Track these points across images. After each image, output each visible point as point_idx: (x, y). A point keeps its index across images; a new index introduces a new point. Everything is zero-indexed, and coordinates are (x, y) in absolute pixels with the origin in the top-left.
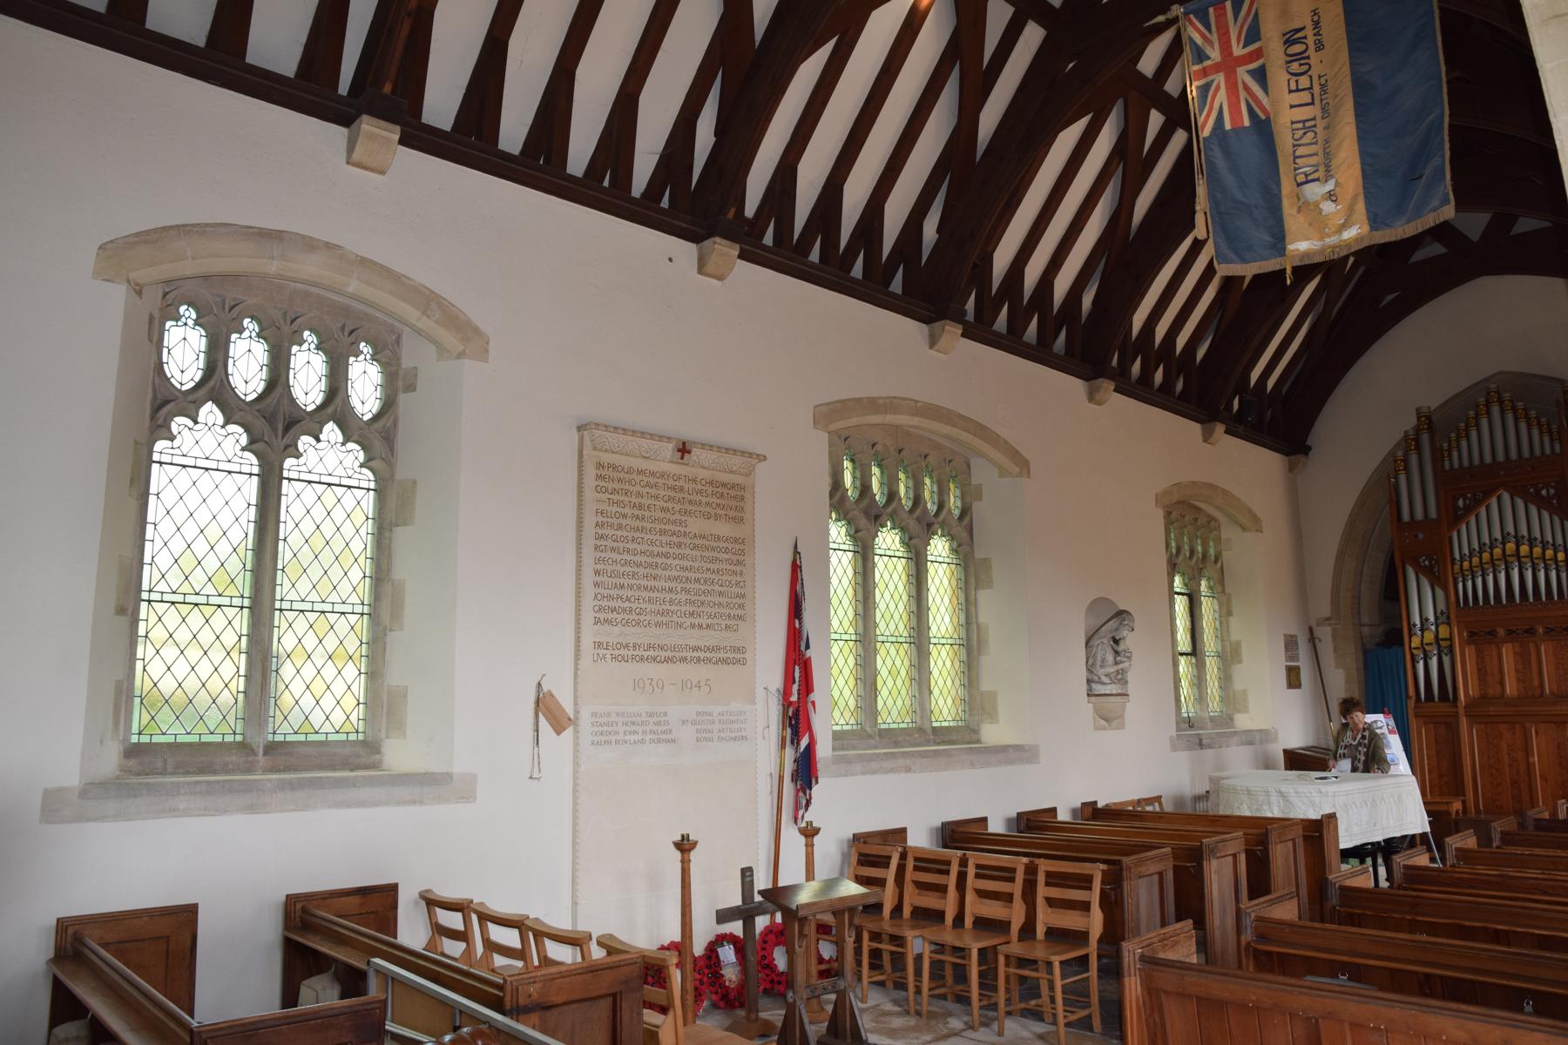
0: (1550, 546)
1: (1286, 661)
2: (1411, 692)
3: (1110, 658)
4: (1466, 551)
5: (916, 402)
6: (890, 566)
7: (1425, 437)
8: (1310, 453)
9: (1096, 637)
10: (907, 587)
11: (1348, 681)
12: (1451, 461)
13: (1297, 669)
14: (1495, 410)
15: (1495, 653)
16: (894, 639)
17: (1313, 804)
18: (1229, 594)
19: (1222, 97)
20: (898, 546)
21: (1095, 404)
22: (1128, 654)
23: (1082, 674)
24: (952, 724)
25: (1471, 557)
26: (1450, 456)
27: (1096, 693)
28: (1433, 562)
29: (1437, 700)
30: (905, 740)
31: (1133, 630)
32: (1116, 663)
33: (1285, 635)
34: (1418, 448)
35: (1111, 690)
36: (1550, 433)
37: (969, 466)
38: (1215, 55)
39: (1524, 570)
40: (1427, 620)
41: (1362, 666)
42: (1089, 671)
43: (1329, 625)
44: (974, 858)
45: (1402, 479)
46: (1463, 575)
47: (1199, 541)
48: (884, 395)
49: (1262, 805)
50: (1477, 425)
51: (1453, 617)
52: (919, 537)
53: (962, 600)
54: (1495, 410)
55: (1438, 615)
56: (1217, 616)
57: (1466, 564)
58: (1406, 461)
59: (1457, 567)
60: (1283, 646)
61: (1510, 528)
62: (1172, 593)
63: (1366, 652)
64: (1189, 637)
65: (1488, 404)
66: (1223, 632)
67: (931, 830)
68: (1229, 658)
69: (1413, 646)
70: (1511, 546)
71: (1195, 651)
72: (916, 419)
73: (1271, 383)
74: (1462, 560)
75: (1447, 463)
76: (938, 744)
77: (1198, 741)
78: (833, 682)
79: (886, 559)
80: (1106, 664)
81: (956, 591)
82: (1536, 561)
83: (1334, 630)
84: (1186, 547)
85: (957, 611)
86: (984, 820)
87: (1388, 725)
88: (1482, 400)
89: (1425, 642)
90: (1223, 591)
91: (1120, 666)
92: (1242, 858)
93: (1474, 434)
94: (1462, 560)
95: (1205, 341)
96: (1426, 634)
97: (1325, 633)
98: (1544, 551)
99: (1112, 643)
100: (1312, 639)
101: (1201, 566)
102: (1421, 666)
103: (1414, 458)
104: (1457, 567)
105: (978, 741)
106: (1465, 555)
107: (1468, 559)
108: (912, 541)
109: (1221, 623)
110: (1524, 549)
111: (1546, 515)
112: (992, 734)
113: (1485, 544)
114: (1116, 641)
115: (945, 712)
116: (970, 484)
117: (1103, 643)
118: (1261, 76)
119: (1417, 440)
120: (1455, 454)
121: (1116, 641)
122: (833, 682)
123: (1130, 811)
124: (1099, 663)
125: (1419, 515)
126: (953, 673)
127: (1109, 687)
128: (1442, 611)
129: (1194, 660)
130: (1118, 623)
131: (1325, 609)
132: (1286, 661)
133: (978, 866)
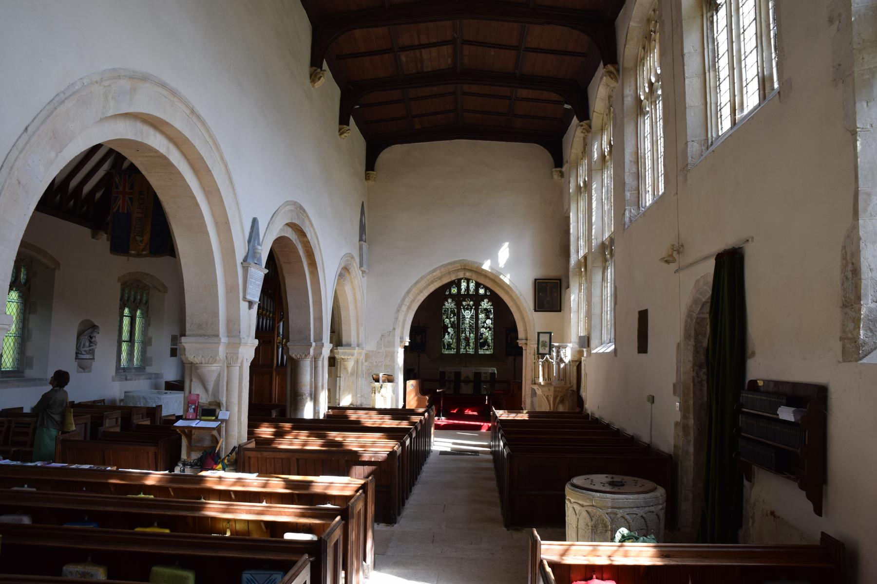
1: (171, 345)
3: (87, 344)
17: (155, 402)
19: (120, 202)
24: (11, 369)
32: (90, 346)
38: (121, 189)
47: (139, 294)
53: (22, 318)
56: (143, 325)
62: (122, 316)
64: (129, 334)
66: (144, 332)
68: (146, 343)
71: (131, 340)
76: (3, 378)
84: (132, 297)
86: (22, 408)
90: (147, 316)
91: (91, 348)
92: (120, 419)
98: (270, 314)
105: (23, 377)
109: (145, 329)
114: (91, 337)
118: (131, 199)
124: (82, 346)
126: (14, 348)
127: (85, 356)
129: (130, 344)
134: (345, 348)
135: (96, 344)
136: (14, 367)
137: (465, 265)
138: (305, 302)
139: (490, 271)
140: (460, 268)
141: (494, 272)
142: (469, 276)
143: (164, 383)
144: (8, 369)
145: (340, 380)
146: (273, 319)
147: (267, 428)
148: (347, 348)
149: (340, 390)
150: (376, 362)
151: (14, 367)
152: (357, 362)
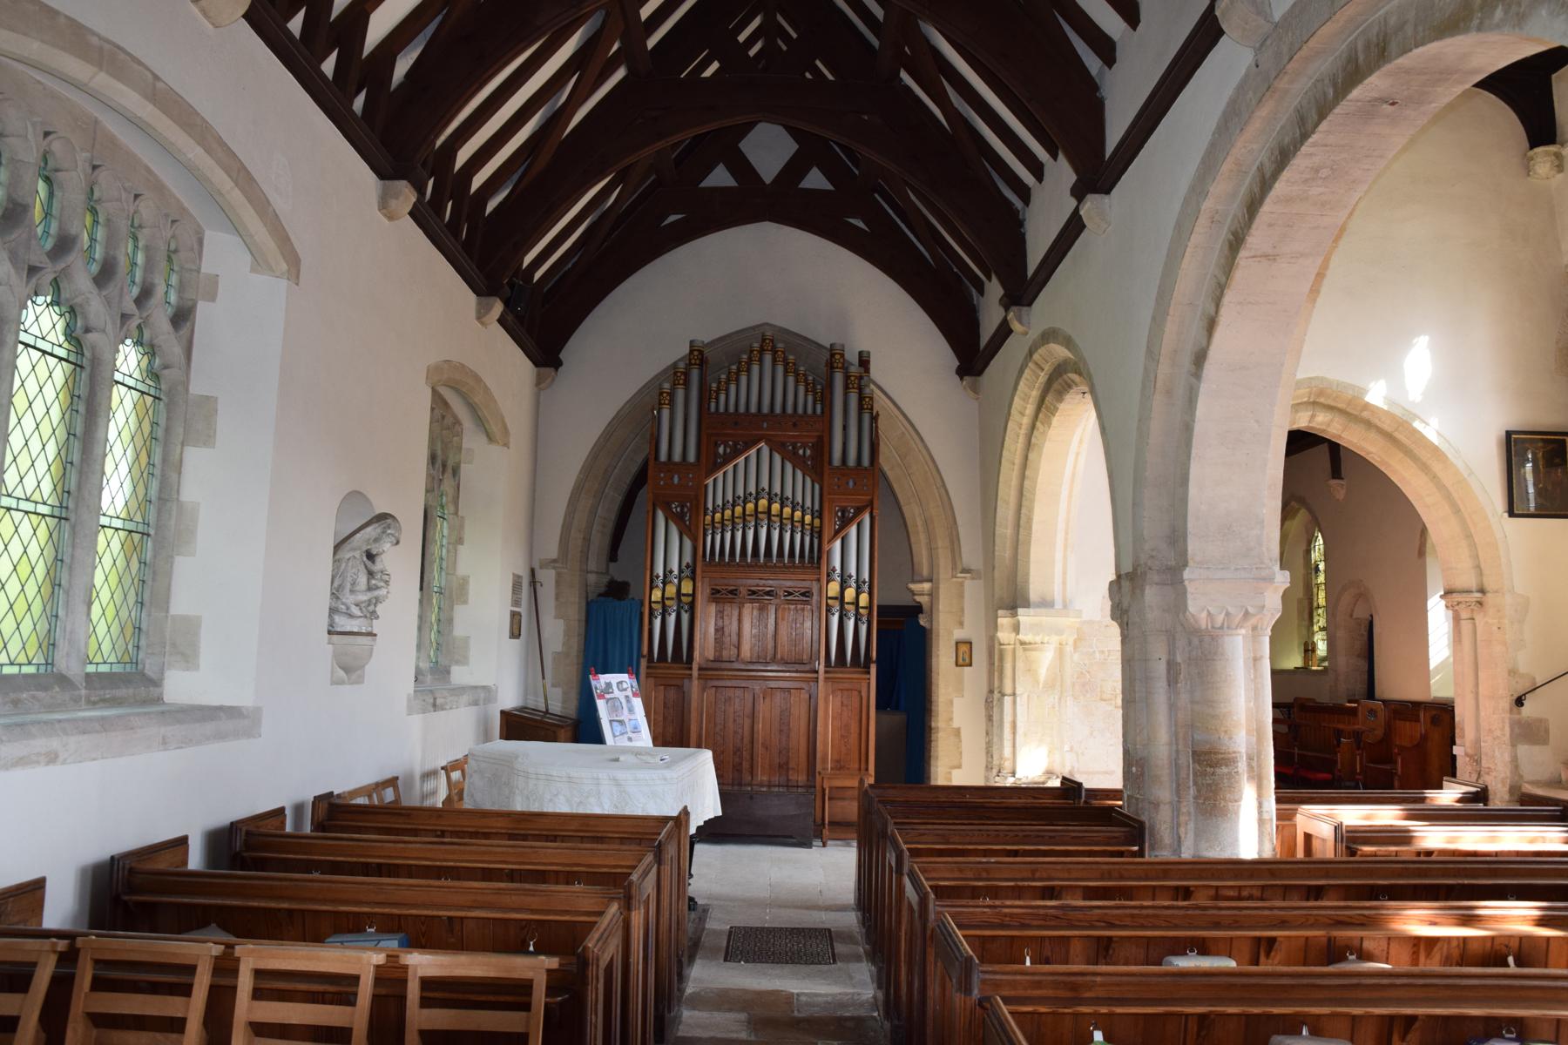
0: (800, 508)
1: (512, 606)
2: (645, 650)
3: (363, 579)
4: (720, 502)
5: (156, 78)
6: (42, 371)
7: (695, 374)
8: (560, 369)
9: (347, 546)
10: (67, 416)
11: (567, 633)
12: (717, 403)
13: (519, 614)
14: (768, 358)
15: (736, 613)
16: (29, 507)
18: (462, 517)
20: (62, 339)
21: (385, 215)
22: (386, 577)
23: (325, 600)
25: (723, 510)
26: (717, 399)
27: (339, 630)
28: (686, 510)
29: (669, 660)
30: (34, 697)
31: (398, 543)
32: (370, 589)
33: (514, 574)
34: (687, 384)
35: (360, 627)
36: (815, 394)
37: (201, 242)
39: (759, 527)
40: (671, 572)
41: (584, 618)
42: (335, 595)
43: (554, 568)
44: (255, 956)
45: (666, 413)
46: (714, 527)
48: (103, 33)
49: (588, 797)
50: (749, 371)
51: (699, 571)
52: (104, 331)
54: (768, 358)
55: (683, 567)
57: (718, 516)
58: (672, 395)
59: (708, 518)
60: (511, 585)
61: (765, 484)
63: (588, 604)
65: (762, 351)
67: (83, 871)
69: (653, 599)
70: (763, 503)
72: (150, 107)
73: (538, 275)
74: (714, 512)
75: (713, 405)
77: (432, 701)
78: (98, 560)
79: (36, 354)
80: (357, 588)
81: (148, 443)
82: (784, 521)
83: (559, 575)
85: (145, 475)
87: (632, 687)
88: (756, 345)
89: (666, 596)
90: (456, 513)
91: (376, 593)
93: (744, 379)
94: (714, 512)
95: (503, 190)
96: (668, 588)
97: (547, 577)
98: (793, 512)
99: (365, 559)
100: (533, 582)
101: (441, 477)
102: (657, 623)
103: (680, 393)
104: (708, 518)
106: (718, 506)
107: (720, 511)
108: (90, 336)
110: (776, 507)
111: (799, 474)
112: (179, 687)
113: (739, 497)
115: (107, 646)
116: (198, 271)
117: (354, 557)
119: (687, 374)
120: (722, 397)
121: (371, 556)
122: (98, 560)
123: (365, 806)
124: (348, 586)
125: (677, 457)
128: (688, 564)
130: (379, 530)
131: (552, 551)
132: (512, 606)
133: (259, 974)
134: (1038, 610)
135: (387, 582)
136: (126, 659)
137: (1321, 393)
138: (1257, 421)
139: (1385, 408)
140: (1306, 399)
141: (1398, 412)
142: (1322, 424)
143: (499, 715)
144: (103, 668)
145: (1014, 702)
146: (817, 533)
147: (1434, 924)
148: (1043, 610)
149: (1014, 733)
150: (1103, 652)
151: (126, 659)
152: (1060, 652)
